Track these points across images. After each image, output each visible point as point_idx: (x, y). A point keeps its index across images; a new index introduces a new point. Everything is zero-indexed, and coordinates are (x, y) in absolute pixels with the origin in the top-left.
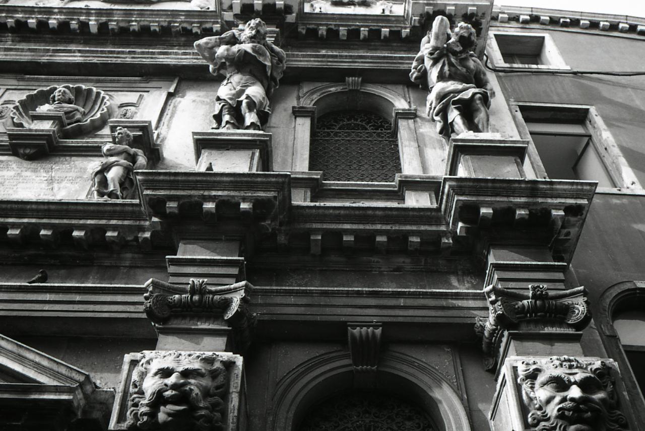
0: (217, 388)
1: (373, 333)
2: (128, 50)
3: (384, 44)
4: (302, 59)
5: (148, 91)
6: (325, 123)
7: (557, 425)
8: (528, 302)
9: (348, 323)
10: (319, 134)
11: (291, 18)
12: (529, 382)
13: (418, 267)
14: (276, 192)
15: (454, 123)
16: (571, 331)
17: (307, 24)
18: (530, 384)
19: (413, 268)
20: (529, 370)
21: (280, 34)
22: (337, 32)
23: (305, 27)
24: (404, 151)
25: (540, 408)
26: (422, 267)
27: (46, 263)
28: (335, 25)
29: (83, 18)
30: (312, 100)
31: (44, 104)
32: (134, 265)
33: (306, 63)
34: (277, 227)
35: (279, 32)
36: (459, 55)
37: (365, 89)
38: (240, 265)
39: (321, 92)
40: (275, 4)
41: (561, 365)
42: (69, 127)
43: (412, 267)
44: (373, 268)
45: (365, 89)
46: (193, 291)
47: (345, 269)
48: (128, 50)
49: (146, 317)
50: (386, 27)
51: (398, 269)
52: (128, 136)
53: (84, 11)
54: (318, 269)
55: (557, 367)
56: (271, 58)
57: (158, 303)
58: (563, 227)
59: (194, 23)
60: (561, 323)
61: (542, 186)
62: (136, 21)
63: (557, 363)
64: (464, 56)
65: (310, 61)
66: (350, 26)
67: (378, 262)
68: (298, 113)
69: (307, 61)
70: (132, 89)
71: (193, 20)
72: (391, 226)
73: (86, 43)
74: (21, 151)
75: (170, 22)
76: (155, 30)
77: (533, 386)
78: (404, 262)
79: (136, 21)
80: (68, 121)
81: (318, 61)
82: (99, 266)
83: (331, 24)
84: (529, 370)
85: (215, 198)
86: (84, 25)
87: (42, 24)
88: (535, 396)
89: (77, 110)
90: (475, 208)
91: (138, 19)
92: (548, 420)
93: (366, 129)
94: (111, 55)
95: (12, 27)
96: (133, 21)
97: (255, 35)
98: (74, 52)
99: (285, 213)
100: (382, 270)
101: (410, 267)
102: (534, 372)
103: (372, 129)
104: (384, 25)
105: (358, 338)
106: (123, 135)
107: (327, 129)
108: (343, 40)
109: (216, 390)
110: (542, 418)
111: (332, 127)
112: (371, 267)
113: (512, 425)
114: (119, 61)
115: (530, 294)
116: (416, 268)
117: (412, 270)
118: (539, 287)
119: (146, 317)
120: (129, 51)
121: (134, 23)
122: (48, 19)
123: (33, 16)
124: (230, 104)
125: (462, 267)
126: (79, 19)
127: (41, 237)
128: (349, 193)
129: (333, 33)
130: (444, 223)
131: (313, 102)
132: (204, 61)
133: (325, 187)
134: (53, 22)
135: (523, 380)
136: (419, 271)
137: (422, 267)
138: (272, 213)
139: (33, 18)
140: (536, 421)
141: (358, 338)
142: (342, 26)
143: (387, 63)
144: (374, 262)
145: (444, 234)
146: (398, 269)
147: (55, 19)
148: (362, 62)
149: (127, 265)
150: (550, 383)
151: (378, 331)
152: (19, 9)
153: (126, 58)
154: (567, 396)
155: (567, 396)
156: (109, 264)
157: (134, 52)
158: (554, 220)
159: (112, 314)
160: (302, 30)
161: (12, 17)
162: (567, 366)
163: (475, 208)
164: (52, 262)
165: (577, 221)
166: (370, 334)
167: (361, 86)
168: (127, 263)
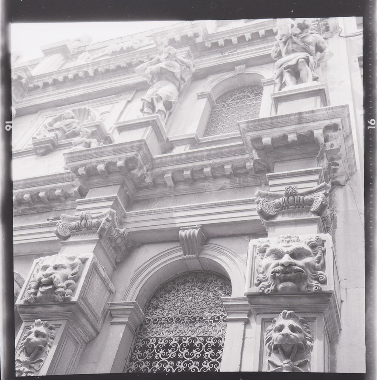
0: (73, 274)
1: (194, 232)
2: (108, 81)
3: (262, 40)
4: (207, 62)
5: (118, 102)
6: (224, 99)
8: (283, 199)
9: (181, 228)
10: (218, 107)
11: (199, 40)
12: (261, 254)
13: (234, 185)
15: (286, 82)
16: (313, 216)
17: (211, 40)
19: (232, 186)
21: (190, 51)
22: (230, 41)
23: (209, 43)
25: (263, 273)
26: (238, 185)
27: (30, 213)
28: (229, 37)
29: (85, 69)
30: (212, 86)
32: (73, 208)
33: (209, 64)
34: (145, 173)
35: (190, 50)
36: (299, 35)
37: (247, 72)
38: (114, 199)
39: (219, 80)
40: (187, 35)
42: (68, 132)
43: (231, 185)
44: (207, 189)
45: (247, 72)
46: (82, 219)
47: (189, 193)
48: (108, 81)
49: (58, 239)
50: (262, 29)
51: (222, 188)
52: (87, 132)
53: (86, 65)
54: (173, 195)
56: (181, 67)
57: (62, 228)
58: (326, 140)
59: (144, 57)
60: (308, 211)
61: (305, 115)
62: (112, 64)
64: (303, 35)
65: (212, 62)
66: (238, 35)
67: (209, 185)
68: (201, 96)
69: (210, 63)
70: (110, 103)
71: (144, 55)
72: (213, 160)
73: (89, 82)
74: (38, 152)
75: (131, 60)
76: (123, 66)
77: (263, 257)
78: (225, 183)
79: (112, 64)
80: (67, 130)
81: (217, 61)
82: (55, 211)
83: (225, 37)
85: (104, 161)
86: (86, 73)
87: (65, 78)
89: (74, 122)
90: (258, 140)
91: (114, 62)
92: (266, 280)
93: (249, 97)
94: (99, 86)
95: (51, 83)
96: (111, 64)
97: (168, 56)
98: (80, 88)
99: (149, 163)
100: (212, 190)
101: (230, 186)
102: (264, 247)
103: (253, 97)
104: (260, 28)
105: (184, 237)
106: (84, 132)
107: (224, 102)
108: (236, 44)
109: (73, 275)
110: (262, 279)
111: (227, 101)
112: (205, 190)
114: (102, 88)
115: (283, 193)
116: (233, 186)
117: (231, 187)
119: (58, 239)
120: (108, 82)
121: (111, 65)
122: (68, 74)
123: (61, 75)
124: (148, 101)
125: (264, 181)
126: (83, 70)
127: (25, 199)
128: (216, 143)
129: (228, 42)
130: (248, 153)
131: (212, 88)
132: (144, 78)
133: (201, 142)
134: (71, 76)
136: (235, 188)
137: (238, 185)
138: (139, 165)
139: (61, 76)
140: (259, 281)
141: (184, 237)
142: (233, 36)
143: (262, 51)
144: (206, 186)
145: (247, 160)
146: (222, 188)
147: (71, 73)
148: (262, 51)
149: (70, 208)
150: (273, 254)
151: (196, 232)
152: (54, 73)
153: (107, 85)
154: (278, 263)
156: (60, 209)
157: (111, 82)
158: (316, 137)
160: (208, 44)
161: (51, 78)
163: (258, 140)
164: (33, 212)
165: (338, 135)
166: (191, 234)
167: (245, 70)
168: (69, 207)
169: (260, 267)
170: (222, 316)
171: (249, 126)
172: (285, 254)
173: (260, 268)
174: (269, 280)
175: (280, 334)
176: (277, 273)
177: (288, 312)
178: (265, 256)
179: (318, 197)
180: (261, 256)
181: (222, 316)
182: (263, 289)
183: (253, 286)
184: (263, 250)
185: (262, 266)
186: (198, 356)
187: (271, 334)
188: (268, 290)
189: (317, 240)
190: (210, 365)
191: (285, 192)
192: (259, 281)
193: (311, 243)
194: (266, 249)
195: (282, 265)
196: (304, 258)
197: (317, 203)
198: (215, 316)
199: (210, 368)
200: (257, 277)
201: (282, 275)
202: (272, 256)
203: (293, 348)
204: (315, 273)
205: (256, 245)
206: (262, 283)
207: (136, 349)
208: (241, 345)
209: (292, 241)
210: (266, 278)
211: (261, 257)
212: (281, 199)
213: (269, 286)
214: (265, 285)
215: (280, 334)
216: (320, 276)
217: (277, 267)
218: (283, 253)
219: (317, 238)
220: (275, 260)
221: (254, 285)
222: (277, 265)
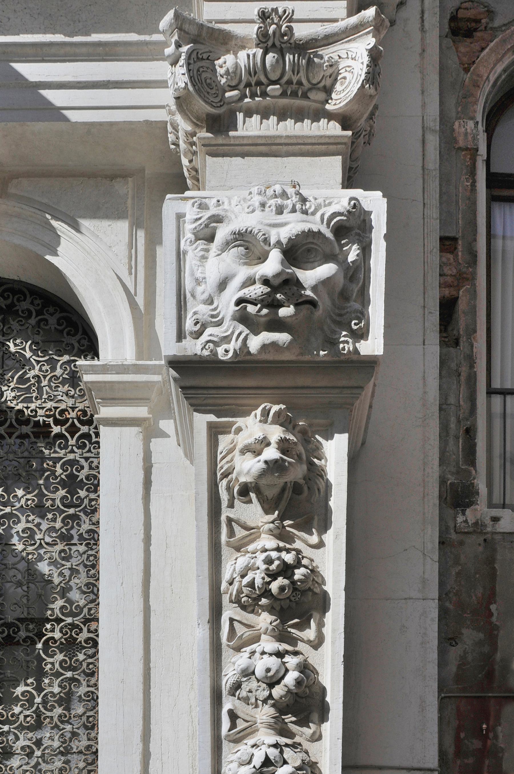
7: (233, 333)
8: (248, 56)
14: (267, 81)
18: (203, 250)
20: (200, 218)
24: (498, 229)
31: (385, 241)
41: (263, 205)
55: (253, 211)
63: (257, 200)
84: (200, 218)
88: (203, 276)
92: (219, 324)
113: (373, 396)
118: (275, 10)
135: (191, 241)
140: (198, 326)
154: (255, 274)
155: (255, 274)
159: (238, 393)
162: (274, 209)
170: (73, 409)
175: (259, 461)
176: (248, 305)
177: (275, 408)
178: (214, 247)
179: (349, 62)
180: (203, 250)
181: (73, 409)
182: (211, 345)
184: (208, 231)
185: (207, 280)
186: (29, 502)
187: (232, 460)
190: (63, 521)
191: (257, 26)
192: (198, 326)
194: (215, 229)
195: (266, 282)
197: (347, 81)
198: (56, 408)
199: (65, 528)
200: (195, 313)
201: (265, 311)
203: (283, 490)
206: (209, 331)
207: (27, 701)
208: (141, 475)
211: (202, 253)
212: (242, 55)
213: (226, 339)
215: (259, 461)
217: (252, 288)
220: (245, 264)
222: (250, 282)
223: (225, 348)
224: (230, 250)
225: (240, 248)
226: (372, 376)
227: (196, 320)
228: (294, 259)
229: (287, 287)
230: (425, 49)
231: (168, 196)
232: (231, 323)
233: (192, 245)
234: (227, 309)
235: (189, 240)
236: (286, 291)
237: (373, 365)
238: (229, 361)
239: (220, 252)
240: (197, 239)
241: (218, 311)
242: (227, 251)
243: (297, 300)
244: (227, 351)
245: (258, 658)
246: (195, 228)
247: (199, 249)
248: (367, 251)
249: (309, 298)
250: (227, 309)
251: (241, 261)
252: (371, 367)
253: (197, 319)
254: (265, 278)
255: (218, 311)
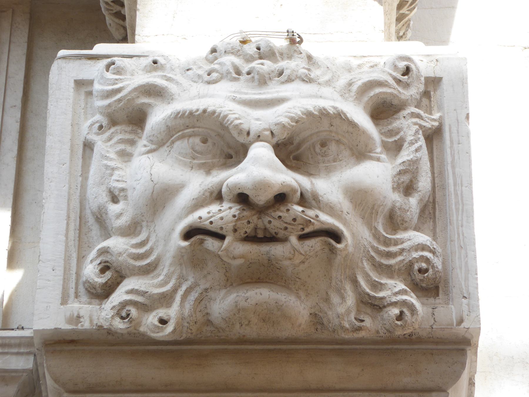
77: (129, 149)
110: (132, 262)
135: (101, 127)
154: (221, 184)
169: (115, 200)
171: (386, 146)
172: (251, 143)
173: (114, 209)
174: (165, 269)
178: (142, 144)
180: (122, 141)
182: (134, 312)
183: (77, 296)
185: (129, 193)
188: (163, 322)
189: (399, 76)
192: (108, 274)
193: (378, 90)
196: (88, 176)
202: (182, 145)
204: (396, 243)
205: (91, 83)
209: (283, 78)
210: (152, 258)
211: (122, 147)
214: (143, 294)
216: (416, 255)
218: (242, 139)
219: (402, 65)
221: (82, 289)
223: (160, 315)
224: (173, 142)
225: (191, 140)
226: (464, 368)
227: (103, 264)
228: (297, 158)
229: (283, 208)
230: (257, 137)
231: (62, 53)
232: (172, 269)
233: (102, 134)
234: (165, 245)
235: (97, 125)
236: (280, 214)
237: (462, 347)
238: (167, 339)
239: (153, 147)
240: (113, 122)
241: (147, 247)
242: (168, 144)
243: (303, 229)
244: (163, 322)
245: (94, 131)
246: (109, 105)
247: (115, 139)
248: (435, 142)
249: (325, 227)
250: (165, 245)
251: (195, 161)
252: (458, 350)
253: (105, 262)
254: (240, 191)
255: (147, 247)
